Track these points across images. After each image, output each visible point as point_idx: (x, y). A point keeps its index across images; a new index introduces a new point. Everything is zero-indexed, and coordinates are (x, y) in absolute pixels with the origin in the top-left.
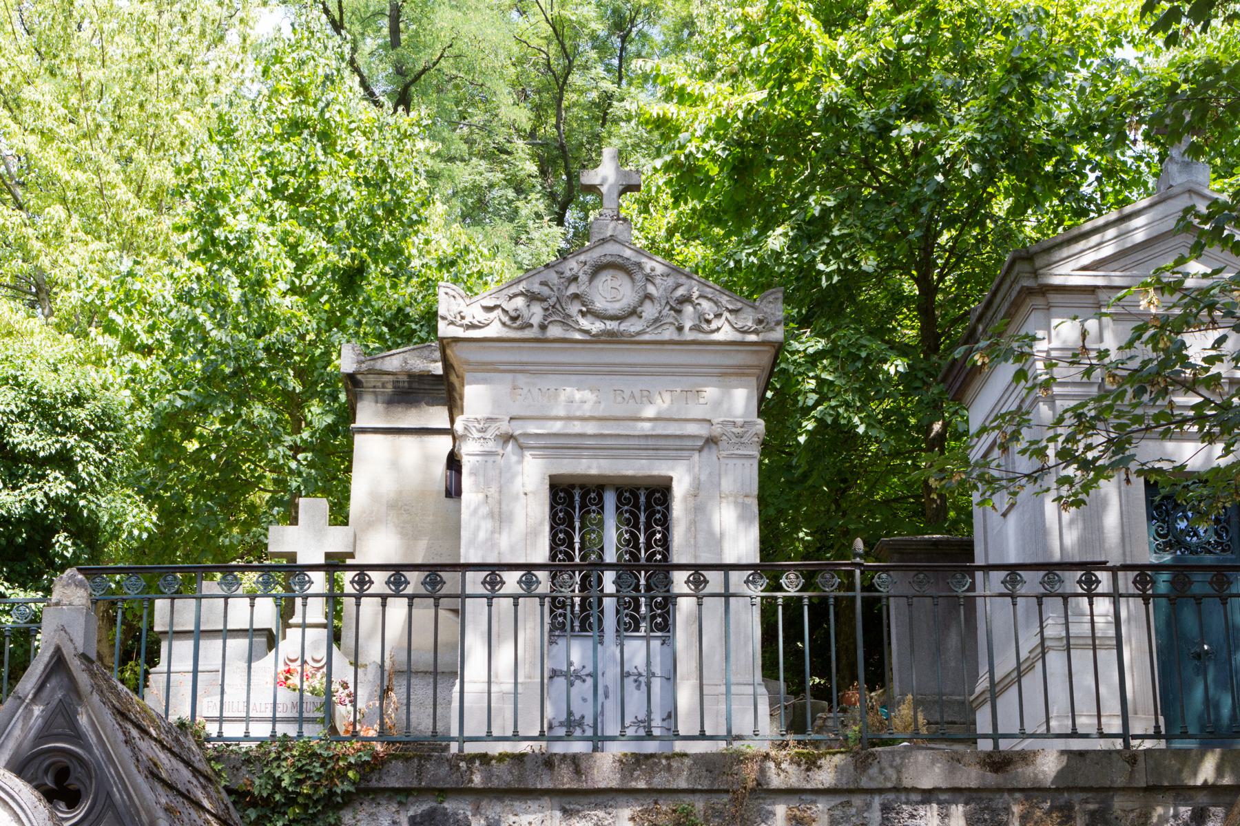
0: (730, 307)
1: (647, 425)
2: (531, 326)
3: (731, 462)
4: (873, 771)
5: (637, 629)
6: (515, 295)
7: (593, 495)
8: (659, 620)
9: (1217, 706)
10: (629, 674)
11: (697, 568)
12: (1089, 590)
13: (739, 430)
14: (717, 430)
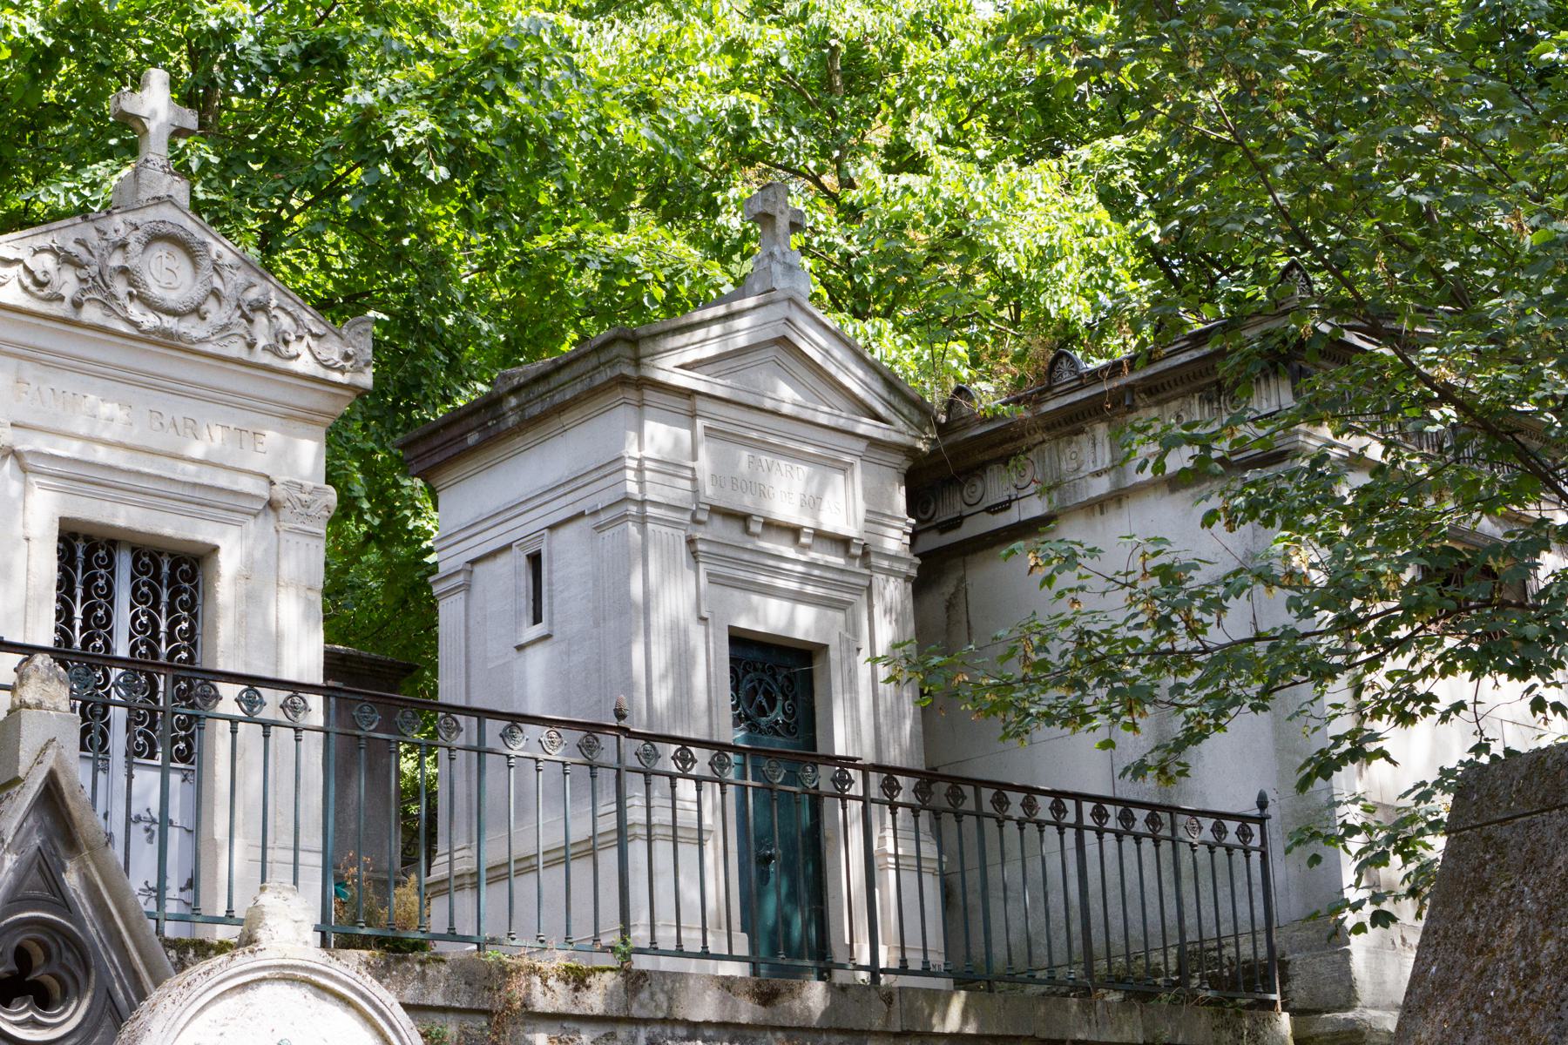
0: (315, 330)
1: (191, 468)
2: (62, 299)
3: (293, 539)
4: (644, 995)
5: (152, 756)
6: (42, 250)
7: (102, 553)
8: (182, 745)
9: (788, 924)
10: (139, 819)
11: (252, 681)
12: (843, 790)
13: (304, 497)
14: (280, 493)
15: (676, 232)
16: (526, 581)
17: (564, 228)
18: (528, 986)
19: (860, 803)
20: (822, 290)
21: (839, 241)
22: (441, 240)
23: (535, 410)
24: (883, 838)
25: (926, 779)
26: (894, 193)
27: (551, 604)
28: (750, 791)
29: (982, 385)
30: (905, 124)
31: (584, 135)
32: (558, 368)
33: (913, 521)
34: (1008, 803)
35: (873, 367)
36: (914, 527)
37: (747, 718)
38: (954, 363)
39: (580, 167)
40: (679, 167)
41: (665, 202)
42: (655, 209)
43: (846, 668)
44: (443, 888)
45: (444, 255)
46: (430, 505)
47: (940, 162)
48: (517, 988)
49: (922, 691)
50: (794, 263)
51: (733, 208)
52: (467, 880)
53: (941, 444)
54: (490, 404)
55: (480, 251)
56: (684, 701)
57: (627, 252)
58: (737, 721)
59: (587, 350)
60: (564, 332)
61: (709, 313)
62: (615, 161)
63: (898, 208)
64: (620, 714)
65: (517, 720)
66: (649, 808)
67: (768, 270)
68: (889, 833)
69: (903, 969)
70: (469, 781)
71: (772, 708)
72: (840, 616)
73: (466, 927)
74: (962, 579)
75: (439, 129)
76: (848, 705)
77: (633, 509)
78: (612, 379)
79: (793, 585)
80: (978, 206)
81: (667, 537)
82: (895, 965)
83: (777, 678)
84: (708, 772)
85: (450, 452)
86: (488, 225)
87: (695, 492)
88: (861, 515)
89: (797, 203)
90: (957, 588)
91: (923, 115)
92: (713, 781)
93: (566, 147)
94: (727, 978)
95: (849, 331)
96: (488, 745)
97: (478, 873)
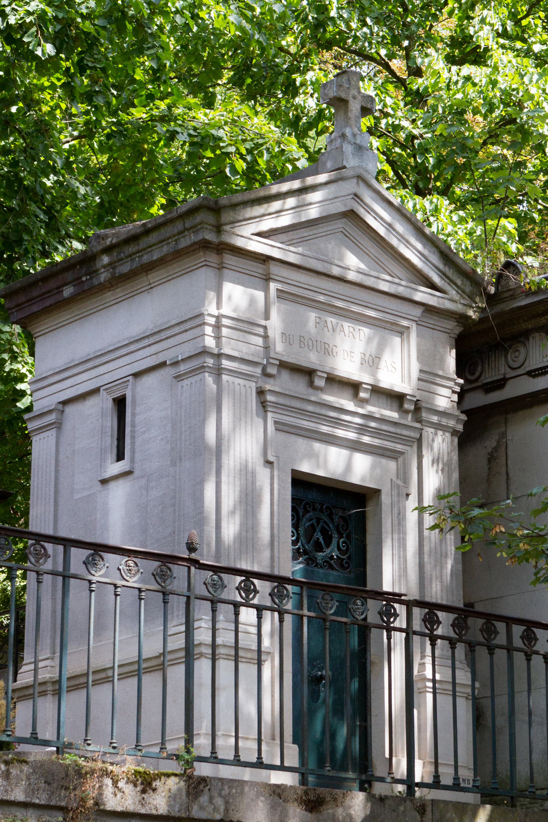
4: (204, 799)
9: (334, 736)
12: (388, 622)
15: (259, 108)
16: (111, 422)
17: (157, 102)
18: (100, 787)
19: (404, 635)
20: (387, 167)
21: (405, 123)
22: (45, 109)
23: (125, 268)
24: (422, 665)
25: (464, 614)
26: (456, 83)
27: (133, 444)
28: (305, 620)
29: (529, 260)
30: (469, 18)
31: (179, 19)
32: (147, 231)
33: (461, 381)
34: (536, 639)
35: (431, 241)
36: (462, 386)
37: (305, 552)
38: (504, 239)
39: (172, 44)
40: (263, 49)
41: (249, 81)
42: (240, 86)
43: (396, 511)
44: (27, 693)
45: (48, 124)
46: (26, 350)
47: (500, 57)
48: (90, 788)
49: (463, 538)
50: (363, 144)
51: (310, 90)
52: (50, 687)
53: (489, 313)
54: (85, 261)
55: (80, 120)
56: (250, 536)
57: (213, 127)
58: (296, 554)
59: (176, 216)
60: (153, 196)
61: (285, 187)
62: (205, 42)
63: (459, 96)
64: (191, 548)
65: (99, 549)
66: (214, 630)
67: (340, 149)
68: (428, 660)
69: (436, 784)
70: (54, 599)
71: (328, 545)
72: (392, 465)
73: (47, 732)
74: (504, 435)
75: (48, 9)
76: (396, 544)
77: (210, 362)
78: (195, 243)
79: (351, 435)
80: (532, 97)
81: (239, 388)
82: (429, 780)
83: (332, 518)
84: (268, 603)
85: (47, 303)
86: (88, 97)
87: (267, 348)
88: (415, 374)
89: (368, 89)
90: (498, 442)
91: (485, 12)
92: (272, 610)
93: (161, 28)
94: (278, 786)
95: (410, 206)
96: (73, 570)
97: (59, 681)
